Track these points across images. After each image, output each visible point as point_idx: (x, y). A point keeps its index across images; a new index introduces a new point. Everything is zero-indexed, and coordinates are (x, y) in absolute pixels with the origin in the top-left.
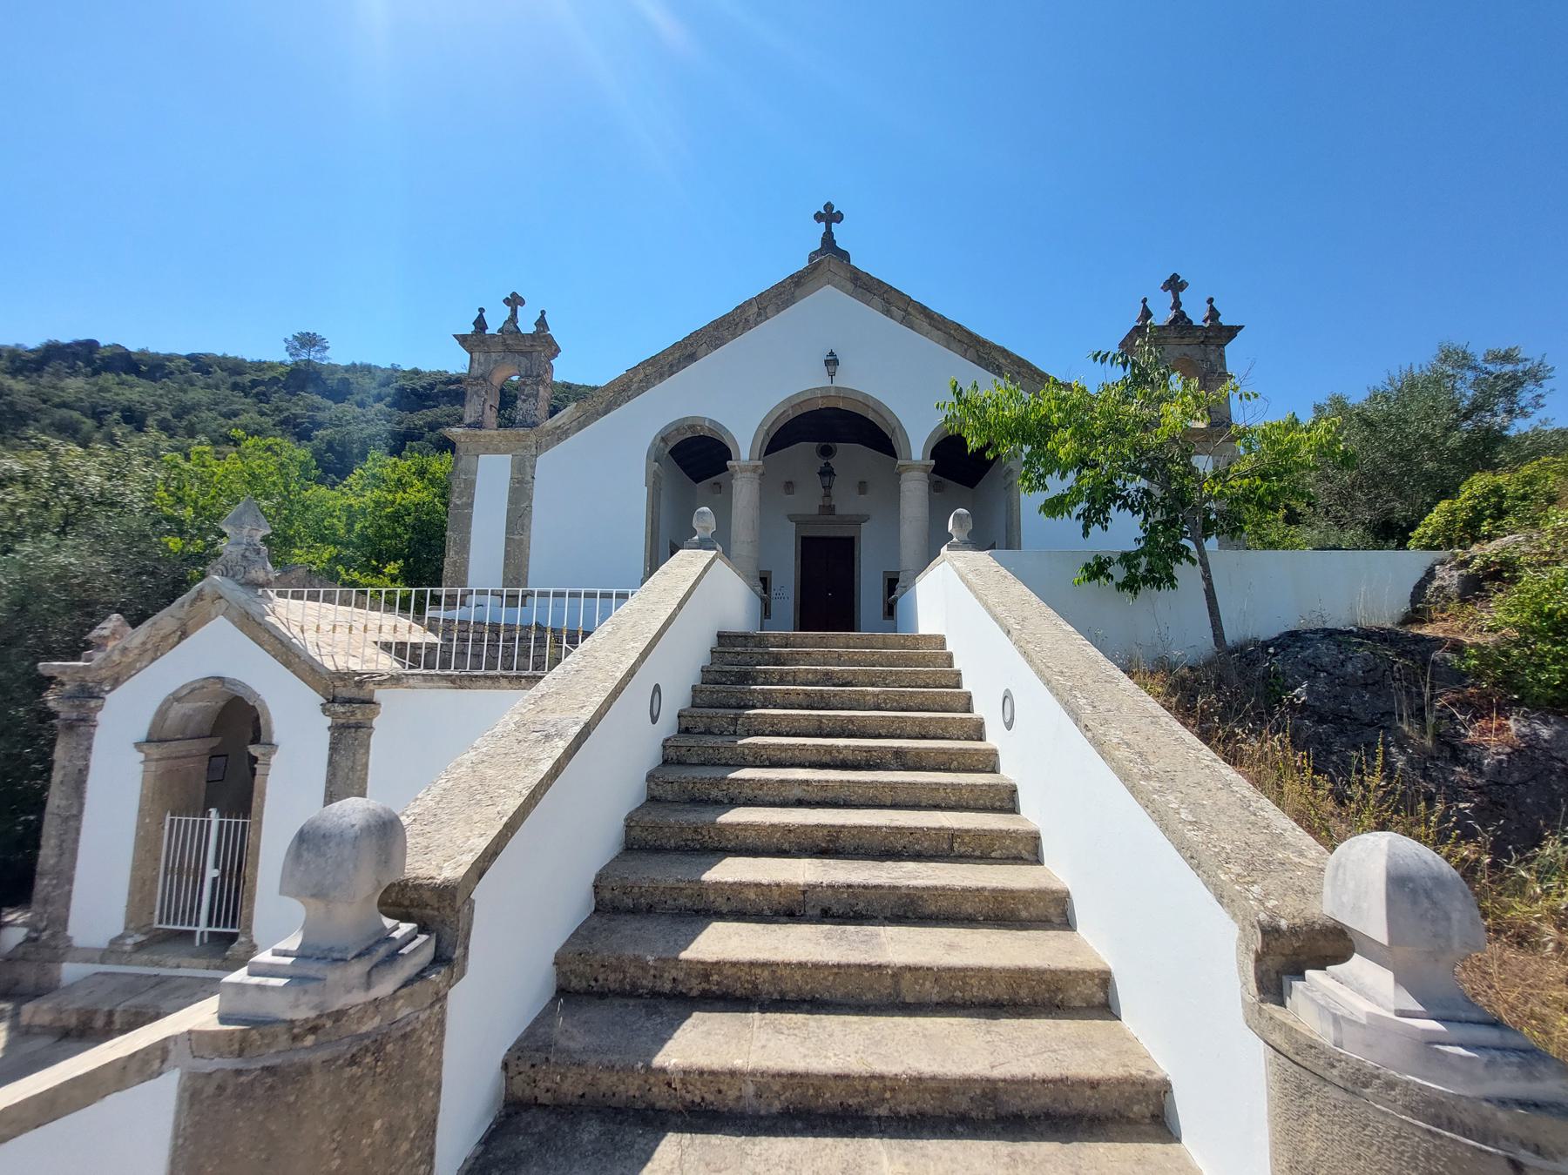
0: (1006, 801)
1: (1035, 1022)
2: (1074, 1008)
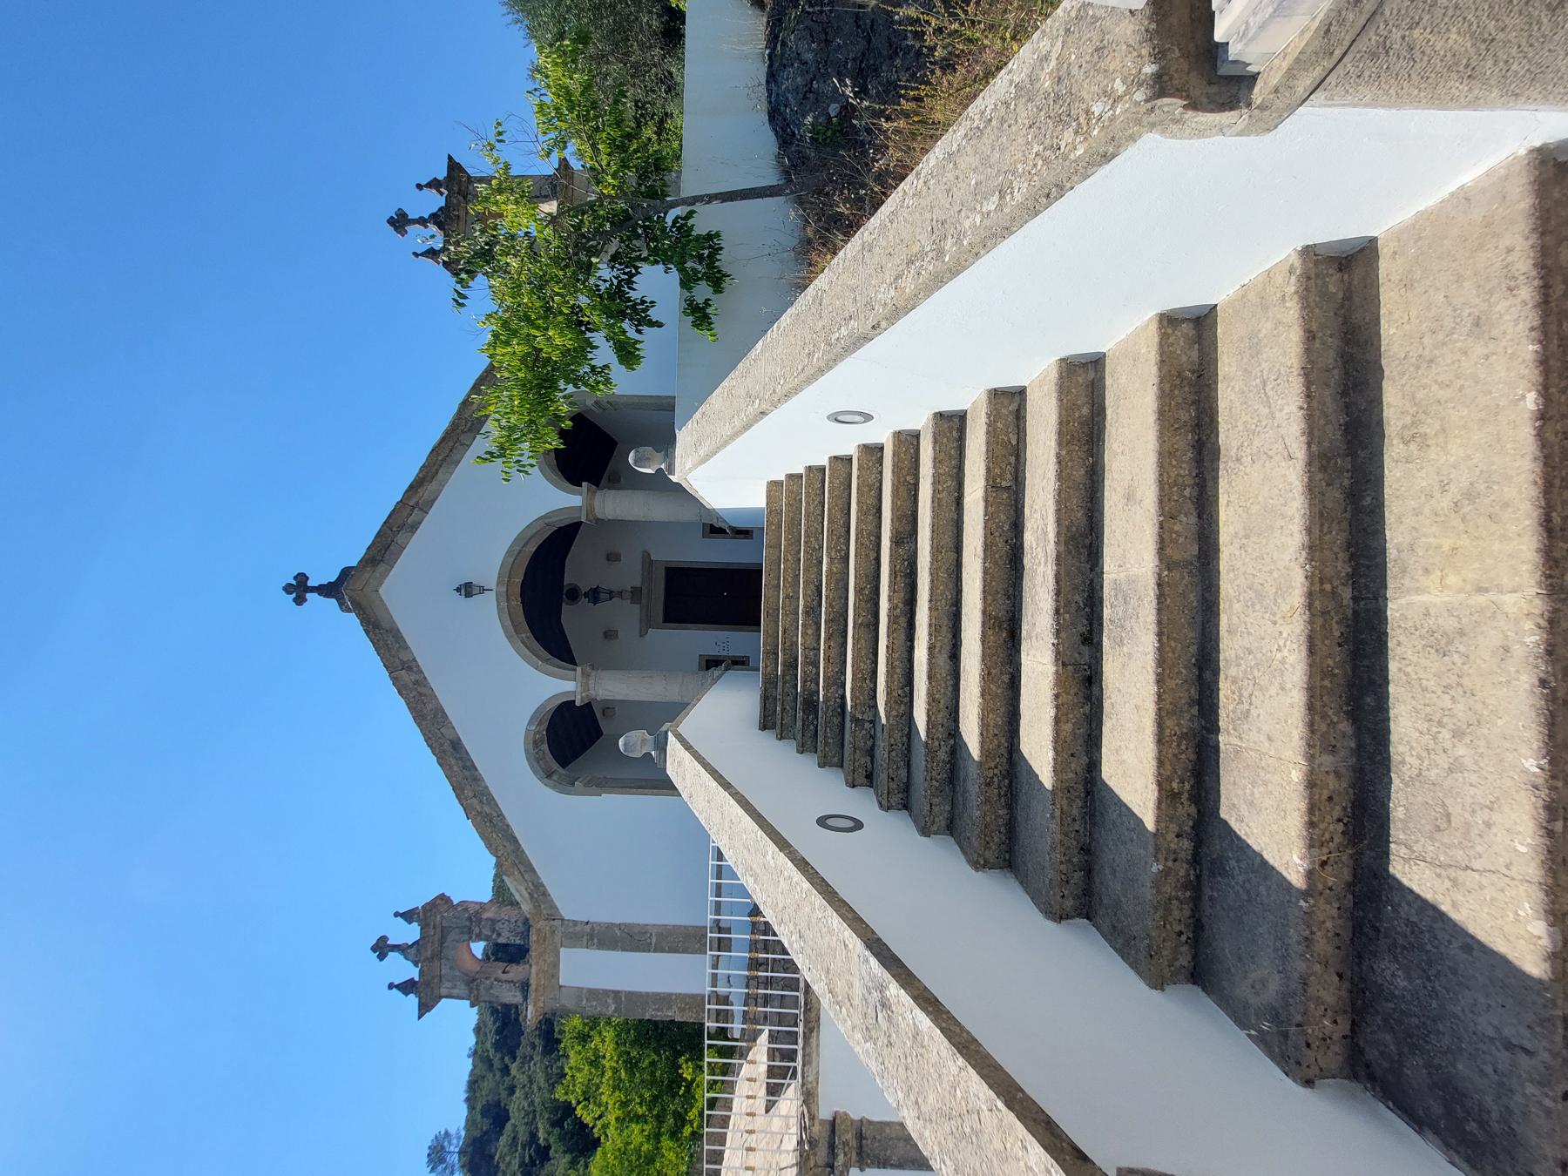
0: (952, 425)
1: (1222, 405)
2: (1201, 358)
